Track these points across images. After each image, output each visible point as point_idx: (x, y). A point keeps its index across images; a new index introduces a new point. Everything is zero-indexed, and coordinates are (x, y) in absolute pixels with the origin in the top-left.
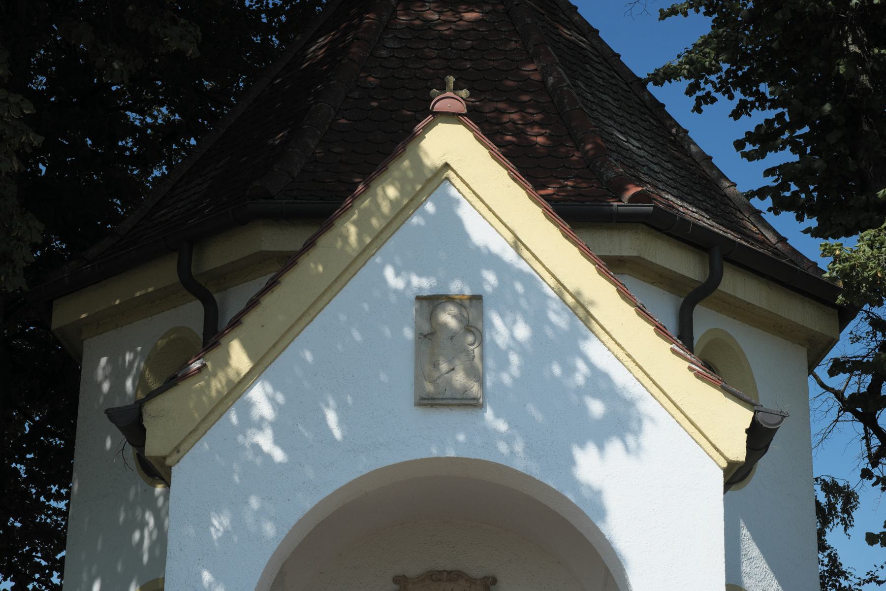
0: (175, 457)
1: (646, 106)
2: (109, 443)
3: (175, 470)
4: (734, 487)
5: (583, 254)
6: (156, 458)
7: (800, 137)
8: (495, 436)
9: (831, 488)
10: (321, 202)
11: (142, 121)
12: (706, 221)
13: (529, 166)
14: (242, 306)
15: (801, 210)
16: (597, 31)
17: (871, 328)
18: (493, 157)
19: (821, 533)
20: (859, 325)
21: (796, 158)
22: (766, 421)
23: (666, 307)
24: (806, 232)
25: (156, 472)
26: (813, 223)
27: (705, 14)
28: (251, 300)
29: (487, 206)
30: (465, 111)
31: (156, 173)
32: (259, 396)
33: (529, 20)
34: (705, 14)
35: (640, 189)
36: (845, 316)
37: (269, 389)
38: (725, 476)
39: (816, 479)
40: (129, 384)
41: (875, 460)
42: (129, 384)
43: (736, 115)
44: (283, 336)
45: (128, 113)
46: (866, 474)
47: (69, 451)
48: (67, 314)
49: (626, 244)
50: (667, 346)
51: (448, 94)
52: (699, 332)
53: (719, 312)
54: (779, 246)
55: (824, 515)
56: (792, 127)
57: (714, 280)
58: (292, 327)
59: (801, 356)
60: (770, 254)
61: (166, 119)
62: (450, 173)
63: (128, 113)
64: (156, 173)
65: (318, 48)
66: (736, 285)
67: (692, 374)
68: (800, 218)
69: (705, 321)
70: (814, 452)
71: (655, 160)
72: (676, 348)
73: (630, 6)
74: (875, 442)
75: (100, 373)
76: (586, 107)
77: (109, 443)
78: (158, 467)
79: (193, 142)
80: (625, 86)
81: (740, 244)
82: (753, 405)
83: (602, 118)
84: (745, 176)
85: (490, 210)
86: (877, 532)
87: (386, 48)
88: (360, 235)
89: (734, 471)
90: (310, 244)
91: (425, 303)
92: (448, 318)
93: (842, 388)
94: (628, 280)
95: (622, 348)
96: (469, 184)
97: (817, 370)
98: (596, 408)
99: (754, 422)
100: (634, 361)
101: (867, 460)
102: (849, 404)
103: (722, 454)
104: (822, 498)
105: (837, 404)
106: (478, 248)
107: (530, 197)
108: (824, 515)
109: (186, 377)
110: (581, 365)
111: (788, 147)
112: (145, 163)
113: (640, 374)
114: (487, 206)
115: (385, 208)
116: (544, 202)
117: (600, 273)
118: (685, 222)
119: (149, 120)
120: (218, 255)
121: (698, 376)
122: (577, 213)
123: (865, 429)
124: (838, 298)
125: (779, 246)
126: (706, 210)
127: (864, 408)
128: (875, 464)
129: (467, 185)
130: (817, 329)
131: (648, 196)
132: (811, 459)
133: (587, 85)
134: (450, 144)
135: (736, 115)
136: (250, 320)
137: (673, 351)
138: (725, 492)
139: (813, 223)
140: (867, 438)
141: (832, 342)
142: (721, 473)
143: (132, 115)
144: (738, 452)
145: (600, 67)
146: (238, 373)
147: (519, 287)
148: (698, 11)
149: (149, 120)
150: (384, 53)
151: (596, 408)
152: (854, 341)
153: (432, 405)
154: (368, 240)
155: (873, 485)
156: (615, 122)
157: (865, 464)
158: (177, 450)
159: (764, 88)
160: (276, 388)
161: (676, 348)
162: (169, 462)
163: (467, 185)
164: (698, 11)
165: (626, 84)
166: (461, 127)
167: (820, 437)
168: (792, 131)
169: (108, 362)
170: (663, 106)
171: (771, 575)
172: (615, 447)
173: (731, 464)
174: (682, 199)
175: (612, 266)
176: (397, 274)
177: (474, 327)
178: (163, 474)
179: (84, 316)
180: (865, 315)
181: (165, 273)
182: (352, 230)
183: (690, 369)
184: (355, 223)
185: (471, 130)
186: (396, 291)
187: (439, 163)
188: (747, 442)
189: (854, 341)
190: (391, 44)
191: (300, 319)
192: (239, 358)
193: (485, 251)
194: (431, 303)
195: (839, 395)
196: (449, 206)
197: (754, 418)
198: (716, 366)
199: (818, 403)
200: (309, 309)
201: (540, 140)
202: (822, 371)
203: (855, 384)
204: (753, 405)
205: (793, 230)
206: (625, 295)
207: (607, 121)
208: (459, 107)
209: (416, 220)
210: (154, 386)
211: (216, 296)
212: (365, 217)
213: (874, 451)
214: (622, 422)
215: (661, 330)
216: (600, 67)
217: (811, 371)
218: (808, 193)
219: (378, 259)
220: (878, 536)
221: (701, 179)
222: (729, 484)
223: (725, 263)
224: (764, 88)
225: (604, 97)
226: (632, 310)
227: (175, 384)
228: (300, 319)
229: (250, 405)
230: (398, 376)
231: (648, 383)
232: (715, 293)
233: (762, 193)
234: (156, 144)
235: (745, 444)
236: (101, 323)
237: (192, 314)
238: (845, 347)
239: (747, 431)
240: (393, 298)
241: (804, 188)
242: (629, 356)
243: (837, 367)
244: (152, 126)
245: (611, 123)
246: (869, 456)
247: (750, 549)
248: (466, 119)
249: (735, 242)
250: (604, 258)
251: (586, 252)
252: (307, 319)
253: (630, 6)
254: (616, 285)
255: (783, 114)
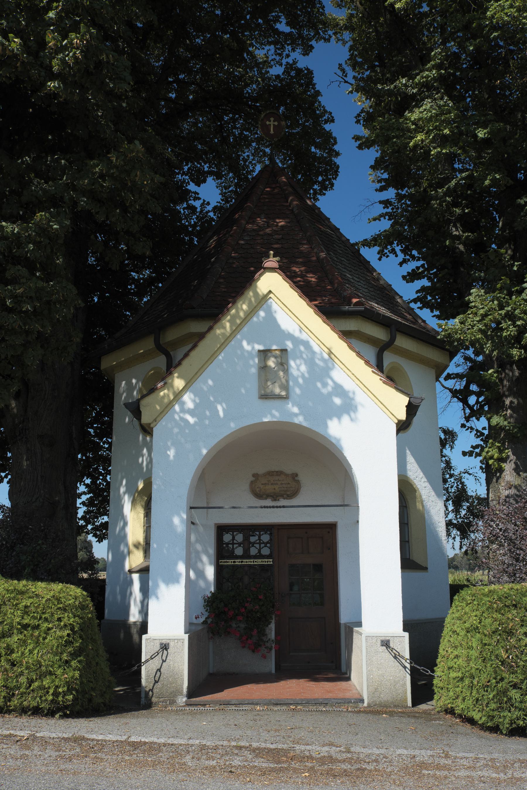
0: (155, 423)
1: (361, 262)
2: (127, 420)
3: (154, 429)
4: (402, 432)
5: (332, 329)
6: (147, 424)
7: (431, 274)
8: (294, 413)
9: (447, 432)
10: (214, 310)
11: (138, 277)
12: (388, 314)
13: (308, 292)
14: (182, 356)
15: (431, 307)
16: (339, 229)
17: (464, 361)
18: (291, 287)
19: (442, 451)
20: (458, 359)
21: (429, 284)
22: (415, 402)
23: (371, 352)
24: (433, 316)
25: (147, 430)
26: (437, 313)
27: (388, 220)
28: (185, 354)
29: (289, 309)
30: (278, 267)
31: (145, 300)
32: (188, 399)
33: (308, 225)
34: (388, 220)
35: (358, 300)
36: (452, 355)
37: (192, 396)
38: (397, 427)
39: (440, 428)
40: (135, 393)
41: (467, 419)
42: (135, 393)
43: (401, 264)
44: (200, 369)
45: (132, 273)
46: (463, 426)
47: (110, 424)
48: (108, 362)
49: (352, 325)
50: (370, 370)
51: (270, 259)
52: (386, 364)
53: (395, 354)
54: (422, 324)
55: (443, 444)
56: (428, 270)
57: (392, 340)
58: (204, 365)
59: (432, 373)
60: (418, 328)
61: (149, 276)
62: (271, 295)
63: (132, 273)
64: (145, 300)
65: (212, 243)
66: (402, 342)
67: (381, 382)
68: (432, 311)
69: (389, 359)
70: (439, 417)
71: (366, 287)
72: (374, 370)
73: (353, 218)
74: (468, 411)
75: (121, 390)
76: (334, 263)
77: (127, 420)
78: (147, 428)
79: (160, 285)
80: (351, 254)
81: (404, 324)
82: (409, 395)
83: (341, 268)
84: (407, 291)
85: (290, 311)
86: (467, 451)
87: (243, 240)
88: (231, 327)
89: (401, 424)
90: (210, 328)
91: (262, 353)
92: (271, 363)
93: (452, 387)
94: (353, 341)
95: (350, 371)
96: (280, 300)
97: (440, 379)
98: (337, 401)
99: (410, 403)
100: (355, 377)
101: (464, 419)
102: (455, 393)
103: (395, 417)
104: (443, 437)
105: (450, 395)
106: (283, 331)
107: (308, 304)
108: (443, 444)
109: (157, 389)
110: (330, 382)
111: (426, 278)
112: (140, 295)
113: (358, 382)
114: (289, 309)
115: (242, 314)
116: (314, 307)
117: (340, 337)
118: (378, 314)
119: (141, 276)
120: (172, 334)
121: (384, 382)
122: (329, 312)
123: (463, 405)
124: (449, 347)
125: (422, 324)
126: (389, 309)
127: (461, 395)
128: (468, 421)
129: (280, 300)
130: (440, 361)
131: (362, 303)
132: (437, 419)
133: (334, 254)
134: (271, 283)
135: (401, 264)
136: (185, 363)
137: (373, 372)
138: (397, 434)
139: (437, 313)
140: (464, 409)
141: (447, 367)
142: (395, 425)
143: (133, 274)
144: (403, 416)
145: (341, 245)
146: (178, 389)
147: (302, 348)
148: (385, 218)
149: (141, 276)
150: (242, 242)
151: (337, 401)
152: (457, 365)
153: (266, 398)
154: (234, 328)
155: (466, 430)
156: (348, 270)
157: (463, 421)
158: (155, 420)
159: (415, 252)
160: (195, 396)
161: (374, 370)
162: (152, 426)
163: (280, 300)
164: (385, 218)
165: (352, 253)
166: (276, 274)
167: (442, 409)
168: (429, 272)
169: (126, 384)
170: (369, 262)
171: (419, 470)
172: (345, 418)
173: (399, 421)
174: (378, 304)
175: (346, 335)
176: (248, 344)
177: (283, 365)
178: (149, 430)
179: (114, 363)
180: (462, 354)
181: (149, 343)
182: (228, 325)
183: (381, 379)
184: (229, 321)
185: (281, 275)
186: (247, 351)
187: (265, 292)
188: (407, 411)
189: (457, 365)
190: (246, 238)
191: (207, 361)
192: (178, 383)
193: (286, 332)
194: (265, 354)
195: (451, 390)
196: (270, 313)
197: (409, 401)
198: (392, 379)
199: (442, 394)
200: (211, 357)
201: (313, 280)
202: (442, 379)
203: (459, 385)
204: (409, 395)
205: (429, 318)
206: (351, 348)
207: (343, 270)
208: (276, 265)
209: (255, 319)
210: (145, 392)
211: (171, 353)
212: (234, 317)
213: (467, 415)
214: (349, 407)
215: (367, 363)
216: (341, 245)
217: (437, 380)
218: (436, 300)
219: (239, 336)
220: (467, 452)
221: (386, 294)
222: (398, 431)
223: (397, 332)
224: (415, 252)
225: (343, 259)
226: (354, 354)
227: (154, 392)
228: (207, 361)
229: (184, 403)
230: (250, 386)
231: (362, 387)
232: (393, 346)
233: (415, 301)
234: (143, 288)
235: (405, 412)
236: (121, 367)
237: (161, 361)
238: (452, 369)
239: (406, 406)
240: (246, 354)
241: (434, 297)
242: (353, 374)
243: (449, 377)
244: (143, 279)
245: (346, 271)
246: (465, 418)
247: (410, 459)
248: (278, 271)
249: (401, 323)
250: (341, 331)
251: (333, 329)
252: (210, 362)
253: (353, 218)
254: (347, 343)
255: (424, 264)
